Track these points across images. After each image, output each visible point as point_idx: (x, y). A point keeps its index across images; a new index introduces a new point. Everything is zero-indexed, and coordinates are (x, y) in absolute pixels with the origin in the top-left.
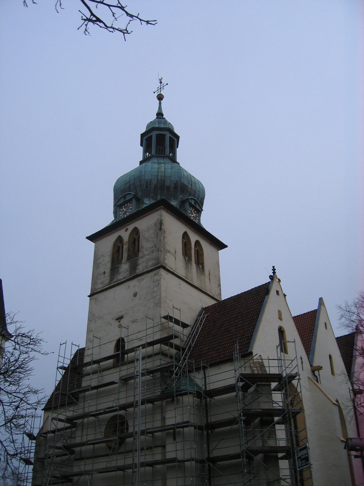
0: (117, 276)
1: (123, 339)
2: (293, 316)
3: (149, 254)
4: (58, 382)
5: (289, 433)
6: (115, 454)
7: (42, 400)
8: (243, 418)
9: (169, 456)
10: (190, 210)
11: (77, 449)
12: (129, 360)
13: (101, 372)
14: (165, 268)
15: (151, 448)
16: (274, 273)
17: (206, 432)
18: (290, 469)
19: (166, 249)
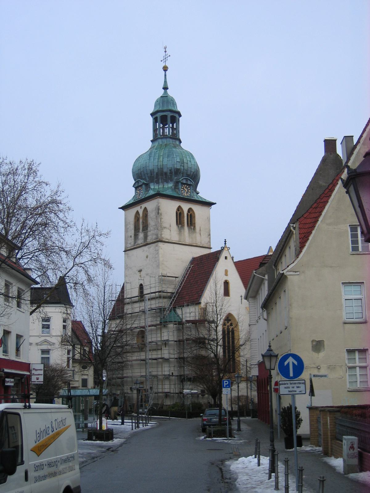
10: (182, 188)
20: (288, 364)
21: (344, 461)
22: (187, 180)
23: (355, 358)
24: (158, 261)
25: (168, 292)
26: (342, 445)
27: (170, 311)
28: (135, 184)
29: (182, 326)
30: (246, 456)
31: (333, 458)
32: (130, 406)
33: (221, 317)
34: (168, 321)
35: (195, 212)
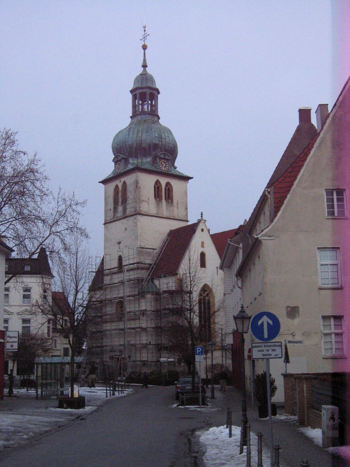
20: (262, 324)
21: (323, 433)
22: (165, 155)
23: (330, 325)
25: (146, 263)
26: (321, 415)
27: (148, 282)
28: (114, 158)
29: (160, 296)
30: (218, 426)
31: (309, 428)
33: (195, 283)
34: (146, 291)
35: (173, 186)
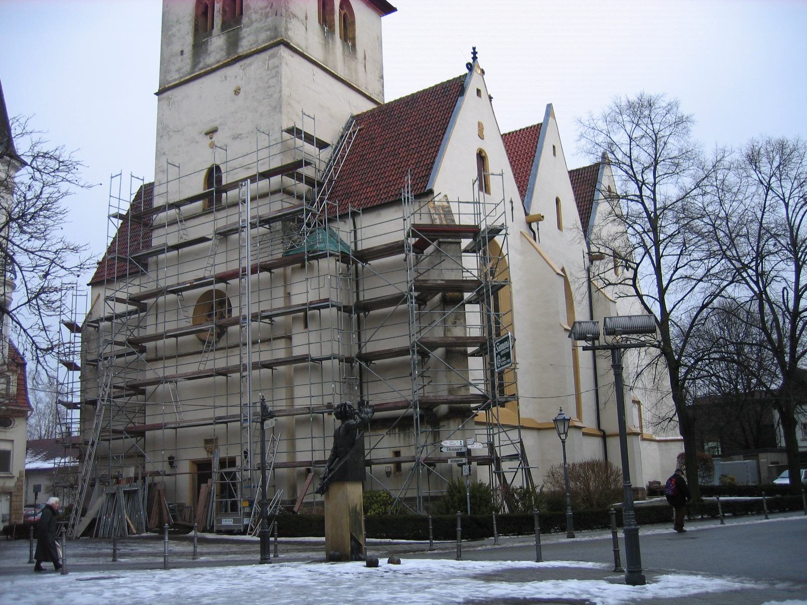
0: (204, 59)
1: (218, 168)
2: (502, 134)
3: (261, 20)
4: (111, 240)
5: (486, 318)
6: (212, 351)
7: (88, 262)
8: (415, 294)
9: (298, 352)
11: (149, 345)
12: (229, 201)
13: (184, 222)
14: (288, 45)
15: (269, 340)
16: (475, 58)
17: (356, 315)
18: (485, 370)
19: (290, 10)
24: (276, 96)
32: (172, 510)
